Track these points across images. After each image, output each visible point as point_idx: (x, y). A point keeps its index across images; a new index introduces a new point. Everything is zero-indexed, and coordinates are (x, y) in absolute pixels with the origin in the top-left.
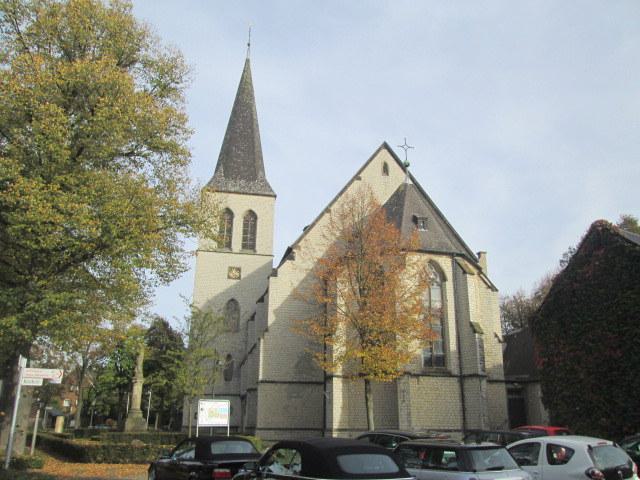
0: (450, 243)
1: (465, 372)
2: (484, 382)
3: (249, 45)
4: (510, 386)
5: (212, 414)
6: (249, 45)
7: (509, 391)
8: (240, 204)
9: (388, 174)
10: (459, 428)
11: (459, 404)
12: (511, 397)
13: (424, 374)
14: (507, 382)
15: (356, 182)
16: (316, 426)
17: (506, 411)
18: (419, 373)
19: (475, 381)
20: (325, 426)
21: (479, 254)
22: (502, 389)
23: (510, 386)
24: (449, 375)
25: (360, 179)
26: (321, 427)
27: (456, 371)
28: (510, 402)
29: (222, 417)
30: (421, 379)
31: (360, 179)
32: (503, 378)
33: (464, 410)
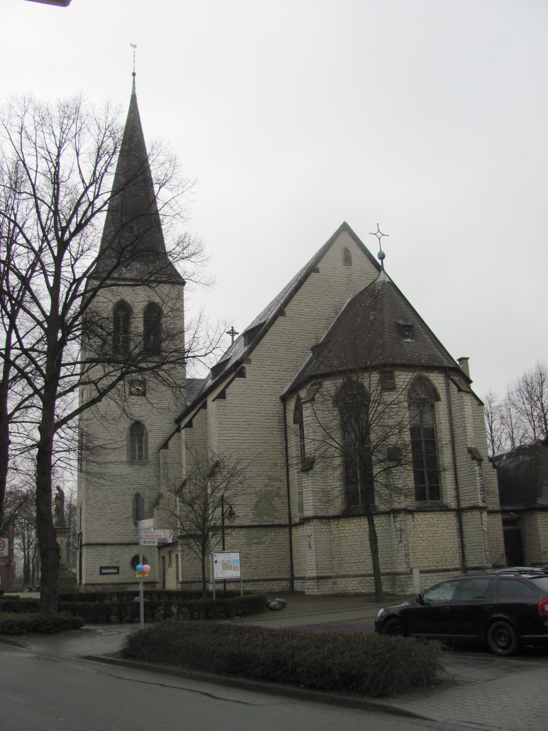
0: (441, 356)
1: (464, 505)
2: (485, 515)
3: (134, 74)
4: (506, 516)
5: (226, 566)
6: (134, 74)
7: (505, 522)
8: (138, 298)
9: (350, 264)
10: (458, 566)
11: (457, 539)
12: (509, 528)
13: (419, 510)
14: (503, 512)
15: (313, 274)
16: (469, 557)
17: (502, 544)
18: (414, 509)
19: (477, 513)
20: (292, 575)
21: (460, 360)
22: (498, 520)
23: (506, 516)
24: (445, 509)
25: (317, 271)
26: (287, 576)
27: (453, 504)
28: (506, 533)
29: (235, 569)
30: (416, 515)
31: (317, 271)
32: (498, 508)
33: (462, 546)
